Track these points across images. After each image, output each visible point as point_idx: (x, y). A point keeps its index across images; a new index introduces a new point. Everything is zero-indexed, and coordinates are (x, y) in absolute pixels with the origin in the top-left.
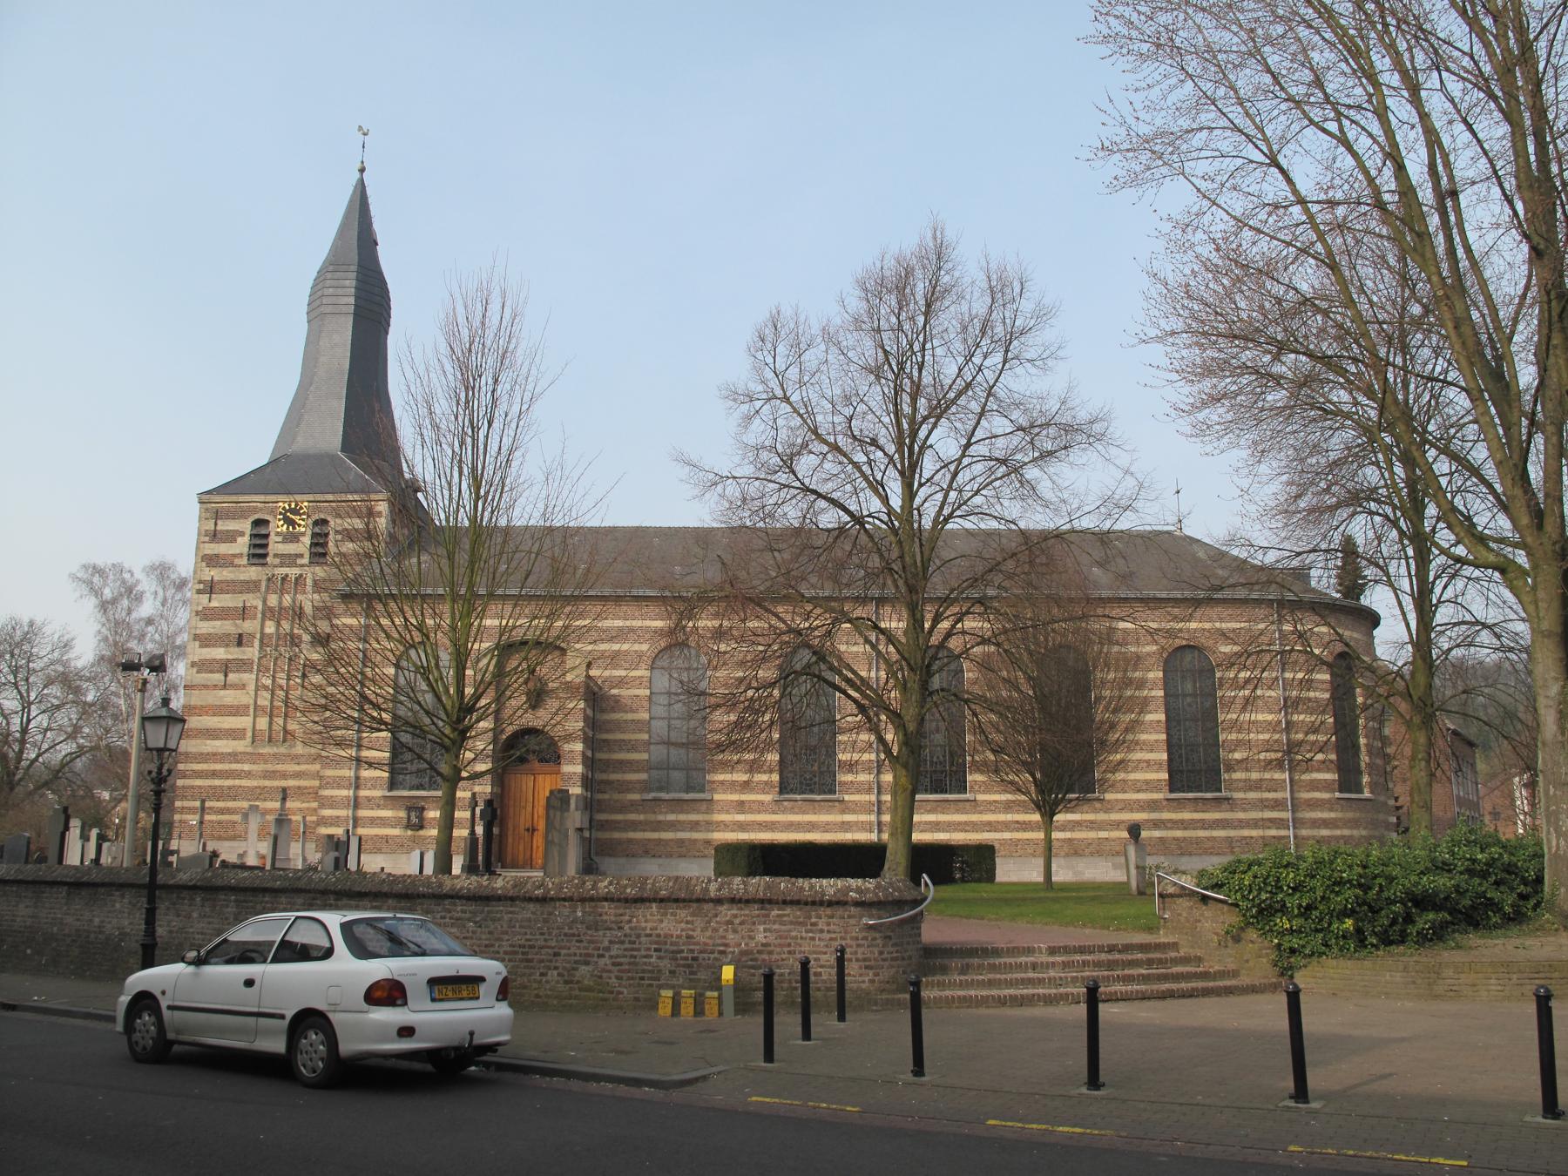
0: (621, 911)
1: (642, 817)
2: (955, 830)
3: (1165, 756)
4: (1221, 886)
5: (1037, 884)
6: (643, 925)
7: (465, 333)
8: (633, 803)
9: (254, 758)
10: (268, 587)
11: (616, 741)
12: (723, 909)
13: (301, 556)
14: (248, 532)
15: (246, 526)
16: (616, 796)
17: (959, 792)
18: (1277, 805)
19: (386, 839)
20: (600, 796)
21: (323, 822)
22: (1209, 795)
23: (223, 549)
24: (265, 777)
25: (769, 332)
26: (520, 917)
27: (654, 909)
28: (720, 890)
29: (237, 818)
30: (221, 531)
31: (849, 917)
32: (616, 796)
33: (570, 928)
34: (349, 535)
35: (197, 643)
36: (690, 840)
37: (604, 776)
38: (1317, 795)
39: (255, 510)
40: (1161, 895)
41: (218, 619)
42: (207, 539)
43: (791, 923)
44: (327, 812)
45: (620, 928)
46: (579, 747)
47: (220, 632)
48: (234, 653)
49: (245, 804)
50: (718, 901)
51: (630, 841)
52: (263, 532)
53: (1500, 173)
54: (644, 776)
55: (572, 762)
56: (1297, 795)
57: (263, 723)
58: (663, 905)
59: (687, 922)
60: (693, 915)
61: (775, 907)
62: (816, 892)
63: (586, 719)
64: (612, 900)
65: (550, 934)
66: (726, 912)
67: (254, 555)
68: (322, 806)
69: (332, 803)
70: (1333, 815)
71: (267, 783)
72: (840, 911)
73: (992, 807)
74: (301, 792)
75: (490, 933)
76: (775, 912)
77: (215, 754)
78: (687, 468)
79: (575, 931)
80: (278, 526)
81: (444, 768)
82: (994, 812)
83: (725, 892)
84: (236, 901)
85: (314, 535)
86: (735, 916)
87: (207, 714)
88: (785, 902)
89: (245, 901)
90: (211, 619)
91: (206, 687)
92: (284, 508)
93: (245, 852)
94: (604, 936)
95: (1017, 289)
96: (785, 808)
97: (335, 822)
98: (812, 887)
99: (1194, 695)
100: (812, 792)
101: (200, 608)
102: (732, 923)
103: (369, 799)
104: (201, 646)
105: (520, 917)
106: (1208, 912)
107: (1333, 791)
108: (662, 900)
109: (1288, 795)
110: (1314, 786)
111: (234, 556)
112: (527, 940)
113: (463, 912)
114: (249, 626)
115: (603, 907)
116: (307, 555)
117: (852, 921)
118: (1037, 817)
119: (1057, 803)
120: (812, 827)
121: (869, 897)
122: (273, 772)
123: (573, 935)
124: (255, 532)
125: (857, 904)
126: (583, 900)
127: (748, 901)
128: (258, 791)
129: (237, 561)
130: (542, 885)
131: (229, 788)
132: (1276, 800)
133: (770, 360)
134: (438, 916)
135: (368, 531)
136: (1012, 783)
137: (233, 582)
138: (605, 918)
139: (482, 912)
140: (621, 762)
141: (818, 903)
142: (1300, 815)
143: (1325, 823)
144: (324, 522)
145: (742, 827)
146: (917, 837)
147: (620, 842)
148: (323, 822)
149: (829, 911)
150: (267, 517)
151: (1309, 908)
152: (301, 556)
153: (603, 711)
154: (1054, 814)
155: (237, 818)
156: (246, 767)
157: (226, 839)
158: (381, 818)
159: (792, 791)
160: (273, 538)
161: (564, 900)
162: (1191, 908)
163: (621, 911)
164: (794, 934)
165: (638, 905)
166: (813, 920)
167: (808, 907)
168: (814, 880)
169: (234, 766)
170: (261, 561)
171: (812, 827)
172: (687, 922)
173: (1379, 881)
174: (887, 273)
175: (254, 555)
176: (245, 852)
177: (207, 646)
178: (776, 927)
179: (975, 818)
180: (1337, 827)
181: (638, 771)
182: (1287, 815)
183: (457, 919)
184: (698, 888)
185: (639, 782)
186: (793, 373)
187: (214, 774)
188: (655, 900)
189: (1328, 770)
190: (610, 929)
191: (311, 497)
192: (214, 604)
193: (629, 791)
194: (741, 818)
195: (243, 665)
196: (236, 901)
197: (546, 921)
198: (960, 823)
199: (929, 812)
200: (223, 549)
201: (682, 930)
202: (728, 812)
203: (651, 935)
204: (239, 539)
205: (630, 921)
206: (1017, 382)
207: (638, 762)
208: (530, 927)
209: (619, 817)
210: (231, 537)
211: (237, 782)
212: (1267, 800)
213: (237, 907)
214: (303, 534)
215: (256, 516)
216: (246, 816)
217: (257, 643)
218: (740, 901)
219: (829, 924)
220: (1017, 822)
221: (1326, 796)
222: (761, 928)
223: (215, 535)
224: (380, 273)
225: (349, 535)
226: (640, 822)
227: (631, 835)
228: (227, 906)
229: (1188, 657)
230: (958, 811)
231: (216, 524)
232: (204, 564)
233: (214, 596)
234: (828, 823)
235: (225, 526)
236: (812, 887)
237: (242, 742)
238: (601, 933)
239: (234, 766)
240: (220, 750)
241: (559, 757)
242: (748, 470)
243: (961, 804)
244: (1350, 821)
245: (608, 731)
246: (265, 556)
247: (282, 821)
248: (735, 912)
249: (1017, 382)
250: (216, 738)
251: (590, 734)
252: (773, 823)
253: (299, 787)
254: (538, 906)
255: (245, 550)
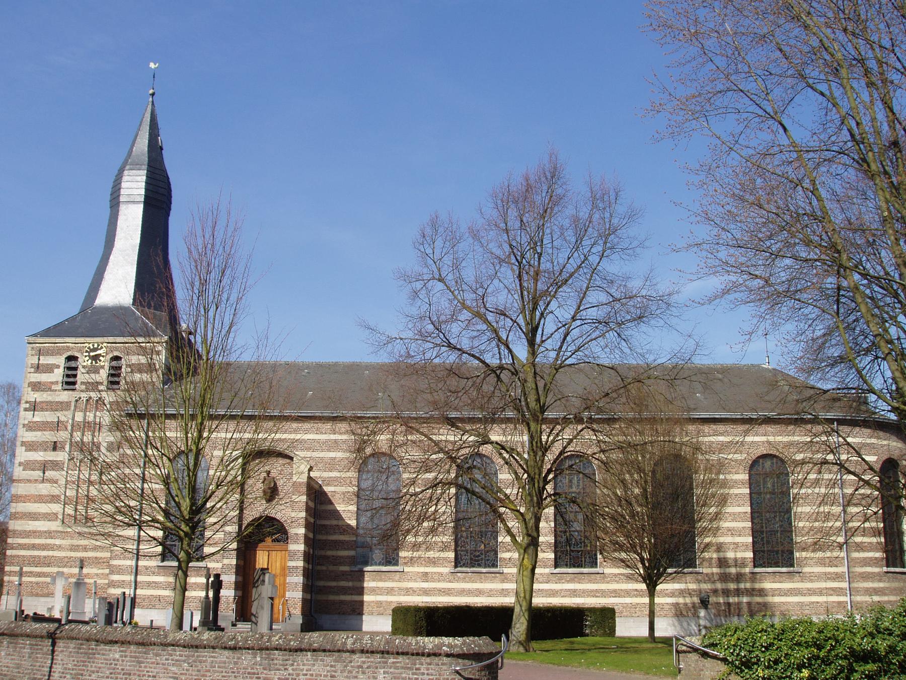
0: (287, 657)
1: (350, 584)
2: (588, 596)
3: (750, 539)
4: (716, 645)
5: (646, 638)
6: (301, 667)
7: (200, 241)
8: (344, 573)
9: (63, 535)
10: (75, 406)
11: (331, 526)
12: (356, 657)
13: (102, 383)
14: (62, 366)
15: (61, 360)
16: (331, 568)
17: (592, 567)
18: (838, 577)
19: (159, 598)
20: (319, 568)
21: (112, 584)
22: (784, 570)
23: (44, 378)
24: (71, 550)
25: (428, 231)
26: (218, 660)
27: (309, 656)
28: (354, 644)
29: (48, 580)
30: (43, 365)
31: (442, 664)
32: (331, 568)
33: (252, 669)
34: (139, 368)
35: (24, 448)
36: (386, 602)
37: (322, 553)
38: (869, 569)
39: (68, 349)
40: (677, 652)
41: (40, 430)
42: (32, 370)
43: (402, 668)
44: (115, 577)
45: (286, 669)
46: (302, 531)
47: (40, 440)
48: (51, 456)
49: (54, 570)
50: (353, 652)
51: (342, 602)
52: (73, 365)
53: (502, 317)
54: (352, 553)
55: (296, 542)
56: (852, 570)
57: (70, 510)
58: (315, 653)
59: (332, 666)
60: (335, 661)
61: (392, 656)
62: (420, 646)
63: (308, 509)
64: (281, 650)
65: (238, 672)
66: (358, 659)
67: (68, 383)
68: (112, 572)
69: (119, 570)
70: (881, 585)
71: (73, 554)
72: (436, 660)
73: (615, 578)
74: (97, 562)
75: (198, 671)
76: (391, 660)
77: (35, 532)
78: (368, 331)
79: (255, 671)
80: (84, 361)
81: (602, 445)
82: (618, 582)
83: (358, 646)
84: (30, 644)
85: (112, 368)
86: (364, 662)
87: (30, 501)
88: (398, 653)
89: (37, 645)
90: (34, 430)
91: (29, 481)
92: (89, 348)
93: (53, 606)
94: (275, 674)
95: (613, 197)
96: (459, 578)
97: (121, 584)
98: (417, 643)
99: (773, 493)
100: (479, 566)
101: (26, 422)
102: (362, 667)
103: (147, 568)
104: (26, 451)
105: (218, 660)
106: (709, 662)
107: (882, 566)
108: (314, 650)
109: (845, 569)
110: (866, 562)
111: (52, 383)
112: (223, 676)
113: (181, 656)
114: (63, 435)
115: (274, 654)
116: (105, 383)
117: (444, 667)
118: (643, 586)
119: (659, 576)
120: (479, 593)
121: (457, 651)
122: (78, 546)
123: (254, 674)
124: (67, 365)
125: (448, 655)
126: (261, 649)
127: (372, 652)
128: (66, 560)
129: (54, 387)
130: (234, 638)
131: (45, 557)
132: (837, 574)
133: (429, 251)
134: (164, 658)
135: (150, 365)
136: (623, 561)
137: (51, 402)
138: (275, 662)
139: (193, 656)
140: (336, 542)
141: (420, 654)
142: (853, 585)
143: (876, 591)
144: (117, 358)
145: (426, 592)
146: (538, 601)
147: (334, 603)
148: (112, 584)
149: (428, 660)
150: (76, 354)
151: (776, 662)
152: (102, 383)
153: (321, 504)
154: (656, 585)
155: (48, 580)
156: (58, 542)
157: (42, 596)
158: (155, 583)
159: (464, 565)
160: (81, 370)
161: (248, 649)
162: (697, 661)
163: (287, 657)
164: (404, 675)
165: (298, 653)
166: (417, 666)
167: (414, 657)
168: (419, 638)
169: (49, 541)
170: (72, 387)
171: (479, 593)
172: (332, 666)
173: (830, 641)
174: (513, 189)
175: (68, 383)
176: (53, 606)
177: (30, 450)
178: (392, 670)
179: (603, 586)
180: (885, 594)
181: (348, 549)
182: (845, 585)
183: (177, 661)
184: (339, 642)
185: (348, 557)
186: (448, 260)
187: (34, 547)
188: (309, 650)
189: (876, 550)
190: (279, 670)
191: (111, 339)
192: (36, 419)
193: (341, 564)
194: (425, 585)
195: (56, 465)
196: (30, 644)
197: (236, 663)
198: (592, 591)
199: (568, 582)
200: (44, 378)
201: (328, 671)
202: (415, 581)
203: (306, 675)
204: (56, 370)
205: (293, 665)
206: (612, 266)
207: (347, 542)
208: (225, 667)
209: (333, 584)
210: (50, 369)
211: (51, 553)
212: (829, 573)
213: (31, 649)
214: (103, 367)
215: (69, 353)
216: (54, 579)
217: (67, 448)
218: (367, 652)
219: (428, 669)
220: (636, 590)
221: (876, 570)
222: (382, 671)
223: (38, 367)
224: (165, 171)
225: (139, 368)
226: (349, 588)
227: (343, 598)
228: (24, 648)
229: (768, 464)
230: (590, 582)
231: (39, 359)
232: (30, 389)
233: (36, 413)
234: (491, 590)
235: (45, 360)
236: (417, 643)
237: (54, 523)
238: (273, 672)
239: (49, 541)
240: (39, 529)
241: (287, 539)
242: (410, 334)
243: (593, 576)
244: (895, 589)
245: (326, 518)
246: (74, 383)
247: (79, 584)
248: (363, 659)
249: (612, 266)
250: (37, 519)
251: (312, 520)
252: (449, 589)
253: (96, 558)
254: (231, 652)
255: (60, 379)
